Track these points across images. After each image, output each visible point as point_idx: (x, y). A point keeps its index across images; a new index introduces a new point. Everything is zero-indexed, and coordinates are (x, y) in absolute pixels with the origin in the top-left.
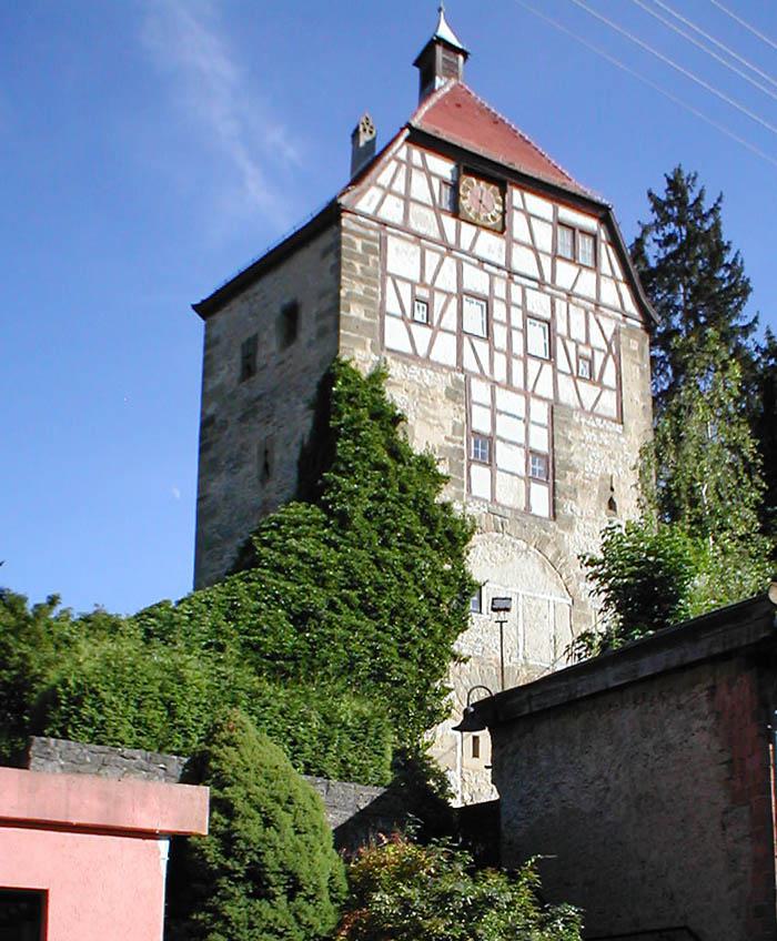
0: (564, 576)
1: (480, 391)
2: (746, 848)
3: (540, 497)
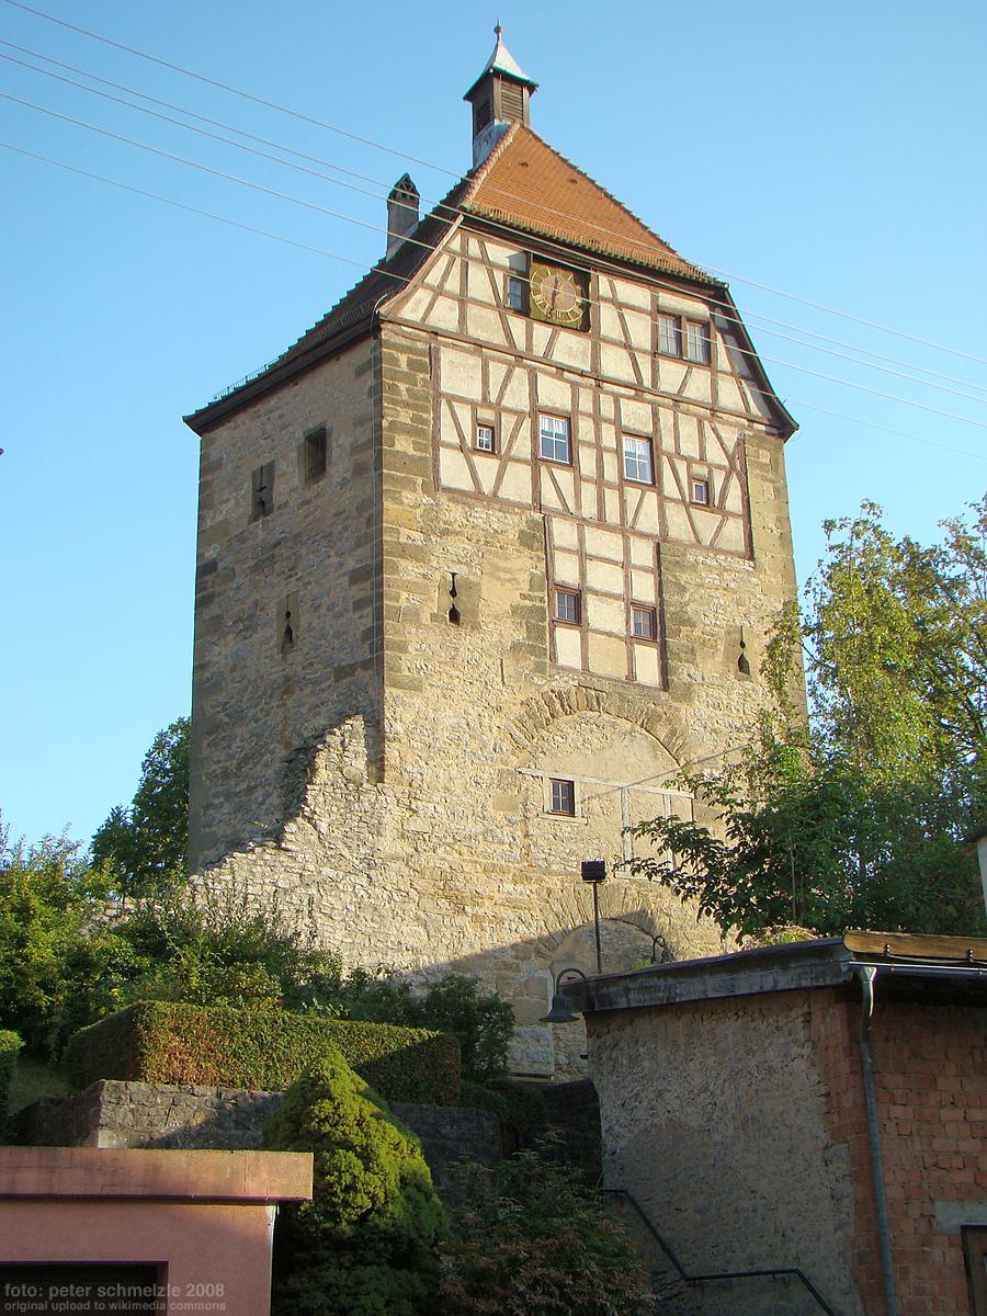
0: (682, 762)
1: (563, 532)
2: (846, 1188)
3: (647, 660)
